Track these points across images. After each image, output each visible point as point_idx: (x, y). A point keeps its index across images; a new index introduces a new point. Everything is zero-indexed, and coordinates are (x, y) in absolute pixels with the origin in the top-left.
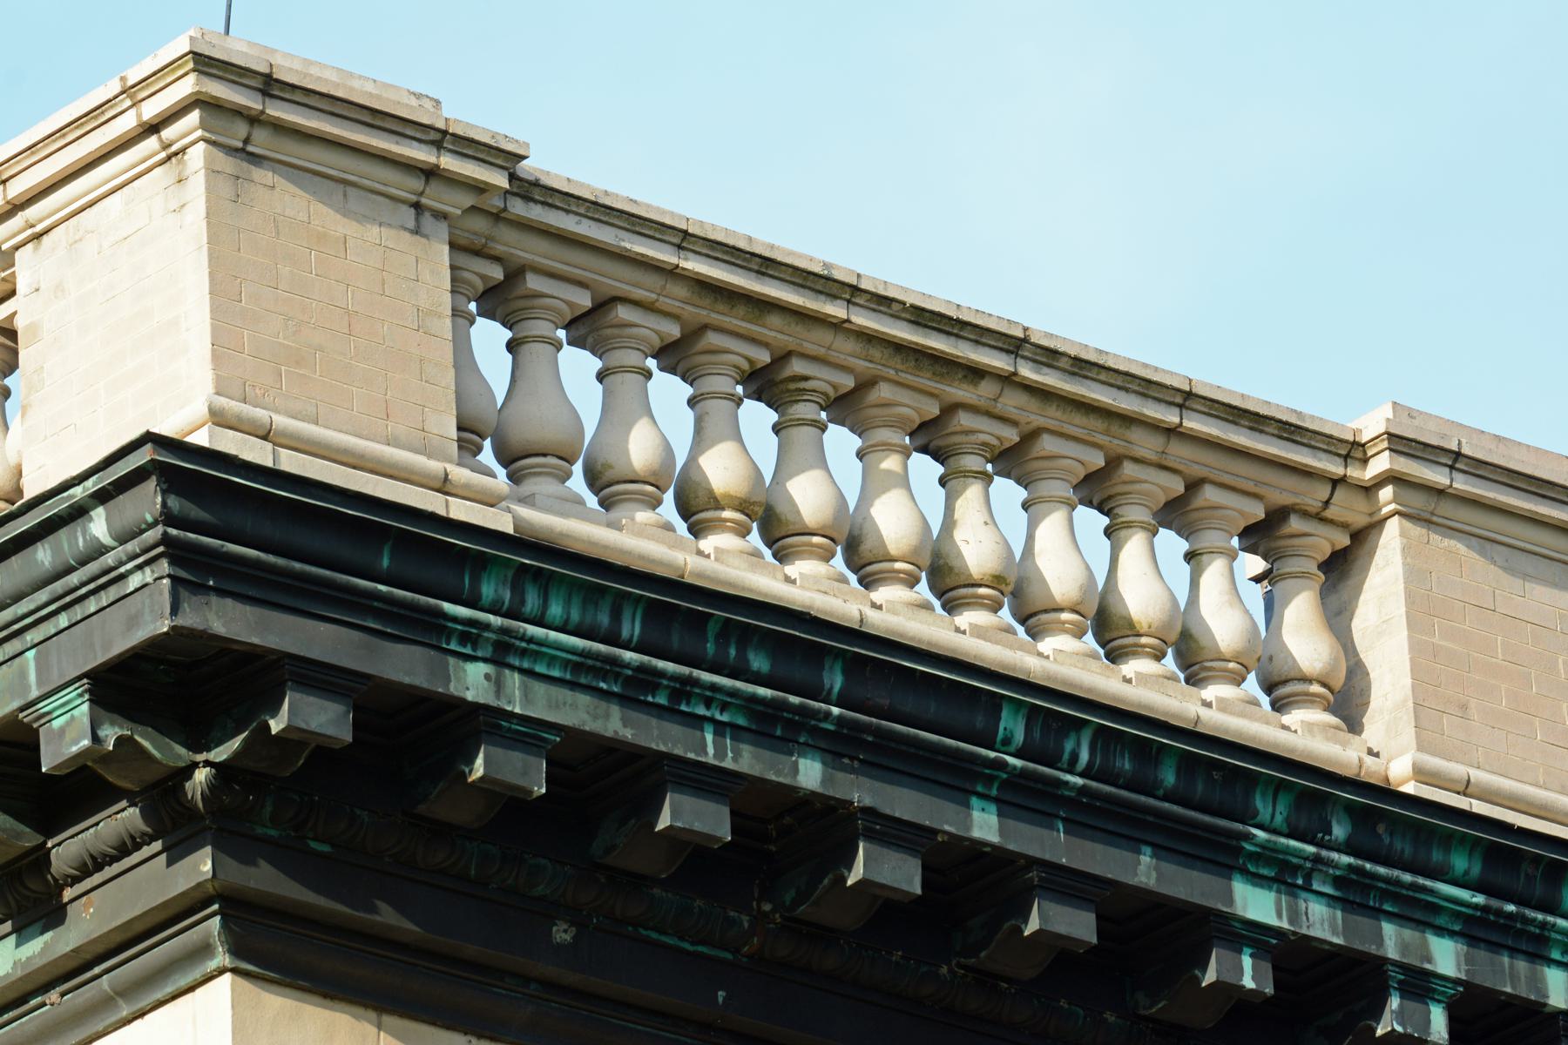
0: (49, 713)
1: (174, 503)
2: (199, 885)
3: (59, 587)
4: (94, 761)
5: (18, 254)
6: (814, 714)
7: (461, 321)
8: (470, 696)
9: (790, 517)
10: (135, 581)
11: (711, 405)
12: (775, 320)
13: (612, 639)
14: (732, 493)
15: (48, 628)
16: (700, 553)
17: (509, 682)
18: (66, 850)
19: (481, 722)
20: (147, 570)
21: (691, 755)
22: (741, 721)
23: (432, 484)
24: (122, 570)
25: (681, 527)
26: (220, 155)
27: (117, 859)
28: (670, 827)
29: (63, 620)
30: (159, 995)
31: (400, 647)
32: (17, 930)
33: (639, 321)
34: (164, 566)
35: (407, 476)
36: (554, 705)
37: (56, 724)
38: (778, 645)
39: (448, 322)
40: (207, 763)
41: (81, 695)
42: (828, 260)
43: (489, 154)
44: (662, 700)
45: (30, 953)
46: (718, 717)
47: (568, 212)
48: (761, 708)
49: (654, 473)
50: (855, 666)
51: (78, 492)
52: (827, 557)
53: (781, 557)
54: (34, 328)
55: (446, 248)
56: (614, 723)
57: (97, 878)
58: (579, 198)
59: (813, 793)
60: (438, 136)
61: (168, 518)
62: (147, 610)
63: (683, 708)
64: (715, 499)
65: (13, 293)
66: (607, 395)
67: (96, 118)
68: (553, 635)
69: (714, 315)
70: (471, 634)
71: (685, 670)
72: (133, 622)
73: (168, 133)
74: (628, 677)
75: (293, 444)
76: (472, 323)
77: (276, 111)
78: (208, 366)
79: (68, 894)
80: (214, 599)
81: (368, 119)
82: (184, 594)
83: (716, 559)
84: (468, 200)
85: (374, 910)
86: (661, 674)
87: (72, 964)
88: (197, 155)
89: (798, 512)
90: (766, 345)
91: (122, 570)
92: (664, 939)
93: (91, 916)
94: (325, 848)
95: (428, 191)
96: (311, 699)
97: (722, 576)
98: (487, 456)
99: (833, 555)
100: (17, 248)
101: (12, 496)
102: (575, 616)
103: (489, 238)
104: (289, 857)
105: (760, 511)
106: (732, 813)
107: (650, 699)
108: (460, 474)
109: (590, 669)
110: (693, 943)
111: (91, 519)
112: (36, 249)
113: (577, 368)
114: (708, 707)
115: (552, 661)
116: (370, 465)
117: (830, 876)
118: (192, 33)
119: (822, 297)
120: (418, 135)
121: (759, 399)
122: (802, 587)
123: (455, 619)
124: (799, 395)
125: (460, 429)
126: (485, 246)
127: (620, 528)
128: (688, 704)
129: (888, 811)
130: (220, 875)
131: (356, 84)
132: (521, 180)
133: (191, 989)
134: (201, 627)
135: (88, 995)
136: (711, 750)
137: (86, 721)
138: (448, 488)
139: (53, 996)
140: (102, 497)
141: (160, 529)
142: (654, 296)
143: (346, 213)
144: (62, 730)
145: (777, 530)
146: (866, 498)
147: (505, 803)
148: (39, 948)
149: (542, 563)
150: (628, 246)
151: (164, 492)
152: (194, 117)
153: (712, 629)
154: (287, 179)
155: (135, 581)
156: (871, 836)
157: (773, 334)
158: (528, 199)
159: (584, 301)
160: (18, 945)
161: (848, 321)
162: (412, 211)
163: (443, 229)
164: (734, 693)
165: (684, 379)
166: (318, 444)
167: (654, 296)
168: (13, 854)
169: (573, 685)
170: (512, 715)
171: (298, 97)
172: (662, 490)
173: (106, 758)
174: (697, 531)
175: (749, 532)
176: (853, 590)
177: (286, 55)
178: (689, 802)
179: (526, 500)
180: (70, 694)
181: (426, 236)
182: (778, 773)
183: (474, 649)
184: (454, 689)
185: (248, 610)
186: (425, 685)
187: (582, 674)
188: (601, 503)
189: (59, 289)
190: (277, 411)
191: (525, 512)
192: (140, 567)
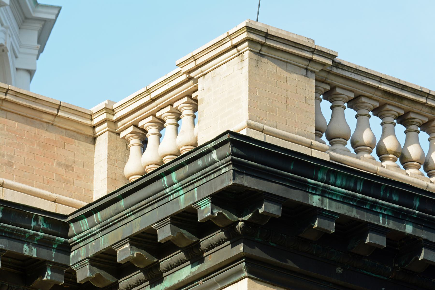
0: (200, 205)
1: (235, 150)
2: (239, 253)
3: (203, 171)
4: (212, 219)
5: (199, 80)
6: (411, 212)
7: (318, 101)
8: (314, 205)
9: (408, 157)
10: (224, 171)
11: (387, 125)
12: (406, 102)
13: (354, 190)
14: (392, 150)
15: (201, 182)
16: (382, 166)
17: (325, 201)
18: (204, 243)
19: (318, 212)
20: (227, 168)
21: (376, 223)
22: (390, 214)
23: (308, 145)
24: (220, 167)
25: (377, 159)
26: (253, 54)
27: (218, 245)
28: (369, 243)
29: (204, 180)
30: (229, 283)
31: (295, 191)
32: (191, 263)
33: (367, 102)
34: (231, 167)
35: (301, 143)
36: (338, 208)
37: (202, 208)
38: (401, 193)
39: (314, 101)
40: (242, 221)
41: (208, 201)
42: (422, 86)
43: (327, 55)
44: (368, 207)
45: (194, 270)
46: (383, 212)
47: (348, 71)
48: (395, 210)
49: (370, 144)
50: (422, 200)
51: (209, 146)
52: (418, 168)
53: (406, 168)
54: (202, 100)
55: (314, 81)
56: (354, 213)
57: (213, 250)
58: (352, 68)
59: (410, 234)
60: (313, 50)
61: (233, 154)
62: (227, 179)
63: (374, 210)
64: (387, 151)
65: (197, 90)
66: (358, 122)
67: (220, 43)
68: (338, 188)
69: (389, 101)
70: (315, 188)
71: (374, 199)
72: (223, 182)
73: (239, 48)
74: (359, 201)
75: (270, 134)
76: (321, 101)
77: (269, 43)
78: (247, 112)
79: (205, 254)
80: (245, 176)
81: (294, 45)
82: (237, 174)
83: (387, 168)
84: (320, 68)
85: (286, 262)
86: (368, 200)
87: (206, 273)
88: (247, 54)
89: (411, 156)
90: (403, 109)
91: (220, 167)
92: (367, 273)
93: (211, 260)
94: (274, 245)
95: (310, 65)
96: (271, 204)
97: (388, 173)
98: (324, 138)
99: (420, 168)
100: (198, 78)
101: (195, 145)
102: (344, 183)
103: (326, 78)
104: (264, 247)
105: (400, 155)
106: (387, 239)
107: (364, 207)
108: (315, 143)
109: (348, 198)
110: (376, 275)
111: (212, 153)
112: (203, 78)
113: (350, 114)
114: (381, 210)
115: (337, 196)
116: (291, 140)
117: (414, 258)
118: (247, 21)
119: (419, 96)
120: (307, 50)
121: (401, 124)
122: (411, 176)
123: (311, 183)
124: (412, 123)
125: (316, 130)
126: (325, 80)
127: (360, 159)
128: (375, 209)
129: (431, 240)
130: (245, 251)
131: (291, 35)
132: (336, 62)
133: (237, 282)
134: (241, 184)
135: (210, 282)
136: (381, 222)
137: (210, 208)
138: (312, 147)
139: (201, 282)
140: (215, 147)
141: (231, 157)
142: (372, 95)
143: (287, 71)
144: (204, 210)
145: (404, 160)
146: (430, 152)
147: (323, 234)
148: (197, 269)
149: (336, 169)
150: (365, 81)
151: (232, 147)
152: (246, 44)
153: (382, 188)
154: (271, 61)
155: (224, 171)
156: (426, 247)
157: (405, 106)
158: (337, 67)
159: (352, 96)
160: (191, 268)
161: (426, 103)
162: (305, 70)
163: (313, 76)
164: (388, 206)
165: (380, 118)
166: (276, 134)
167: (372, 95)
168: (191, 243)
169: (343, 203)
170: (326, 210)
171: (275, 39)
172: (372, 148)
173: (215, 218)
174: (382, 160)
175: (396, 161)
176: (425, 178)
177: (272, 27)
178: (374, 236)
179: (334, 150)
180: (206, 201)
181: (309, 77)
182: (400, 229)
183: (316, 192)
184: (310, 203)
185: (254, 180)
186: (302, 201)
187: (346, 199)
188: (355, 152)
189: (209, 89)
190: (266, 125)
191: (333, 154)
192: (225, 167)
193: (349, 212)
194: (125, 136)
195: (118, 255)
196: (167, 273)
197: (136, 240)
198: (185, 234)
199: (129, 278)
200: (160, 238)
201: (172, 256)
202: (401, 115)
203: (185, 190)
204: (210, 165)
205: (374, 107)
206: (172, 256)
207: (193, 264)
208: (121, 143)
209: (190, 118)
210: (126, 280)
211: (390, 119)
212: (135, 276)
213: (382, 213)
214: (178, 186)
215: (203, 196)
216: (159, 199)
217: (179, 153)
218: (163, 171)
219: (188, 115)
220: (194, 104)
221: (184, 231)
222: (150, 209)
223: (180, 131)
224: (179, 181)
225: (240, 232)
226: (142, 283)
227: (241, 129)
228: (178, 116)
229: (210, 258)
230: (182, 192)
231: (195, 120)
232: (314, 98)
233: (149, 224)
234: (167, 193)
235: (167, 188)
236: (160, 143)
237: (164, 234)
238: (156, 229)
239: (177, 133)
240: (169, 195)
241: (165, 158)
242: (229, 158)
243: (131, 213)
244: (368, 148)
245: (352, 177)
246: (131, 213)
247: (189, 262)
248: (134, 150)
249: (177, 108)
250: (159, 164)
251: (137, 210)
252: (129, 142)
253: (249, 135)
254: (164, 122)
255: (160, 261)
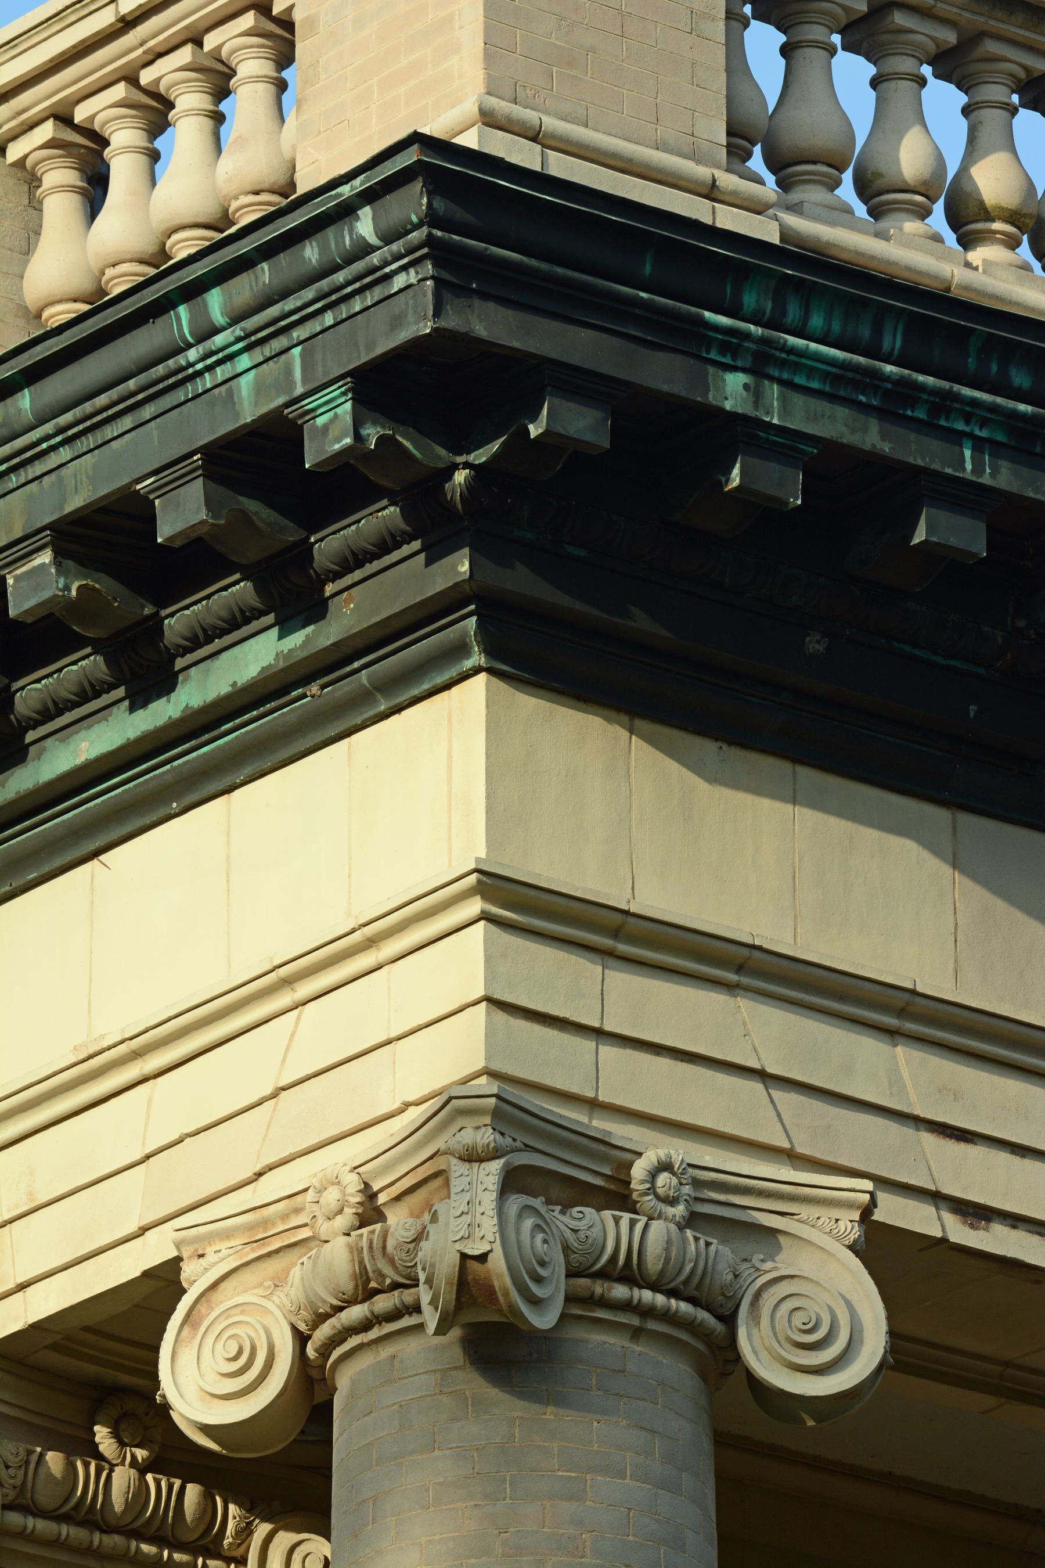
1: (439, 204)
2: (456, 584)
3: (325, 284)
7: (735, 24)
10: (399, 282)
15: (315, 326)
16: (968, 265)
17: (768, 392)
18: (328, 545)
19: (742, 433)
21: (949, 471)
22: (1000, 437)
24: (387, 270)
25: (950, 238)
27: (378, 556)
29: (329, 319)
31: (660, 355)
33: (914, 27)
34: (429, 268)
35: (674, 181)
37: (320, 421)
39: (721, 25)
40: (467, 465)
41: (344, 394)
44: (921, 414)
45: (292, 646)
46: (977, 432)
49: (925, 183)
51: (345, 191)
54: (311, 22)
56: (872, 437)
57: (358, 575)
61: (432, 219)
62: (410, 311)
63: (943, 422)
64: (986, 210)
66: (881, 103)
68: (813, 346)
69: (992, 23)
70: (732, 344)
71: (945, 384)
72: (396, 322)
75: (562, 146)
76: (746, 25)
78: (481, 66)
79: (329, 589)
80: (477, 302)
82: (447, 295)
83: (984, 272)
86: (922, 388)
91: (387, 270)
92: (917, 652)
93: (350, 613)
94: (581, 553)
96: (570, 404)
97: (989, 289)
98: (757, 162)
99: (1018, 244)
102: (836, 327)
105: (1031, 223)
107: (909, 413)
108: (728, 181)
111: (358, 218)
113: (851, 73)
114: (967, 422)
115: (811, 372)
123: (716, 328)
127: (887, 238)
128: (947, 419)
133: (447, 686)
134: (463, 330)
136: (969, 466)
137: (349, 419)
138: (716, 194)
139: (314, 688)
140: (369, 196)
141: (425, 230)
144: (326, 427)
149: (809, 274)
155: (399, 282)
164: (994, 408)
166: (596, 150)
169: (832, 398)
170: (770, 424)
172: (933, 200)
173: (369, 456)
174: (967, 242)
178: (946, 518)
179: (794, 208)
180: (334, 392)
182: (1037, 490)
183: (734, 359)
185: (510, 314)
186: (684, 394)
187: (841, 386)
188: (870, 212)
190: (547, 113)
191: (793, 221)
192: (404, 268)
193: (853, 430)
194: (26, 156)
195: (10, 590)
196: (190, 658)
197: (76, 537)
198: (256, 513)
199: (50, 675)
200: (167, 529)
201: (208, 597)
202: (1036, 75)
203: (258, 355)
204: (349, 261)
205: (938, 47)
206: (208, 597)
207: (286, 626)
208: (11, 182)
209: (265, 91)
210: (38, 681)
211: (995, 92)
212: (74, 668)
213: (971, 436)
214: (232, 339)
215: (325, 374)
216: (161, 386)
217: (225, 219)
218: (166, 287)
219: (257, 79)
220: (282, 40)
221: (252, 505)
222: (127, 422)
223: (230, 140)
224: (234, 321)
225: (460, 506)
226: (97, 695)
227: (458, 129)
228: (220, 82)
229: (347, 601)
230: (244, 361)
231: (285, 97)
232: (723, 15)
233: (125, 480)
234: (191, 365)
235: (190, 346)
236: (153, 183)
237: (182, 512)
238: (151, 497)
239: (218, 149)
240: (199, 374)
241: (175, 237)
242: (415, 236)
243: (58, 439)
244: (919, 198)
245: (864, 303)
246: (58, 439)
247: (270, 618)
248: (60, 207)
249: (216, 55)
250: (91, 300)
251: (81, 427)
252: (40, 180)
253: (486, 150)
254: (171, 105)
255: (164, 613)
